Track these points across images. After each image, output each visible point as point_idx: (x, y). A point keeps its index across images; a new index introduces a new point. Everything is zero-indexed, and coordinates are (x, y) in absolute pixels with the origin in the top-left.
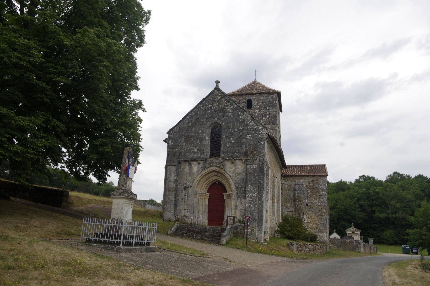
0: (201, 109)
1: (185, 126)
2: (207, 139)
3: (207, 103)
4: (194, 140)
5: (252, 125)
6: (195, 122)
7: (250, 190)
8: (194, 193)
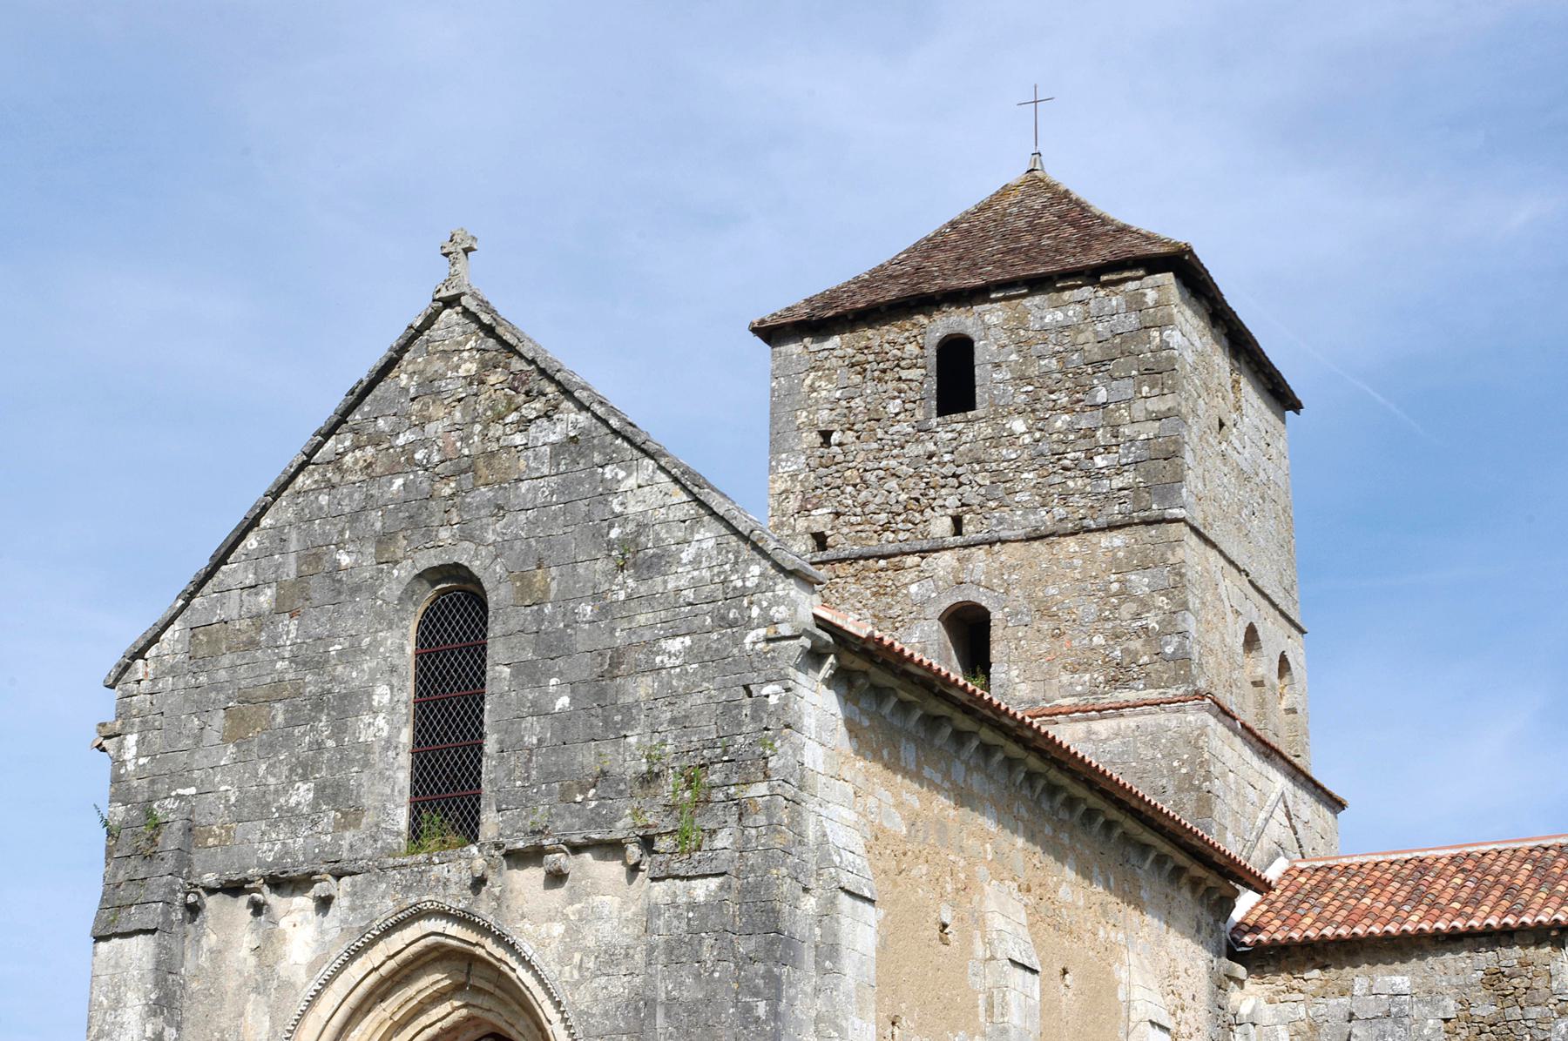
1: (235, 615)
2: (386, 699)
5: (696, 562)
6: (300, 576)
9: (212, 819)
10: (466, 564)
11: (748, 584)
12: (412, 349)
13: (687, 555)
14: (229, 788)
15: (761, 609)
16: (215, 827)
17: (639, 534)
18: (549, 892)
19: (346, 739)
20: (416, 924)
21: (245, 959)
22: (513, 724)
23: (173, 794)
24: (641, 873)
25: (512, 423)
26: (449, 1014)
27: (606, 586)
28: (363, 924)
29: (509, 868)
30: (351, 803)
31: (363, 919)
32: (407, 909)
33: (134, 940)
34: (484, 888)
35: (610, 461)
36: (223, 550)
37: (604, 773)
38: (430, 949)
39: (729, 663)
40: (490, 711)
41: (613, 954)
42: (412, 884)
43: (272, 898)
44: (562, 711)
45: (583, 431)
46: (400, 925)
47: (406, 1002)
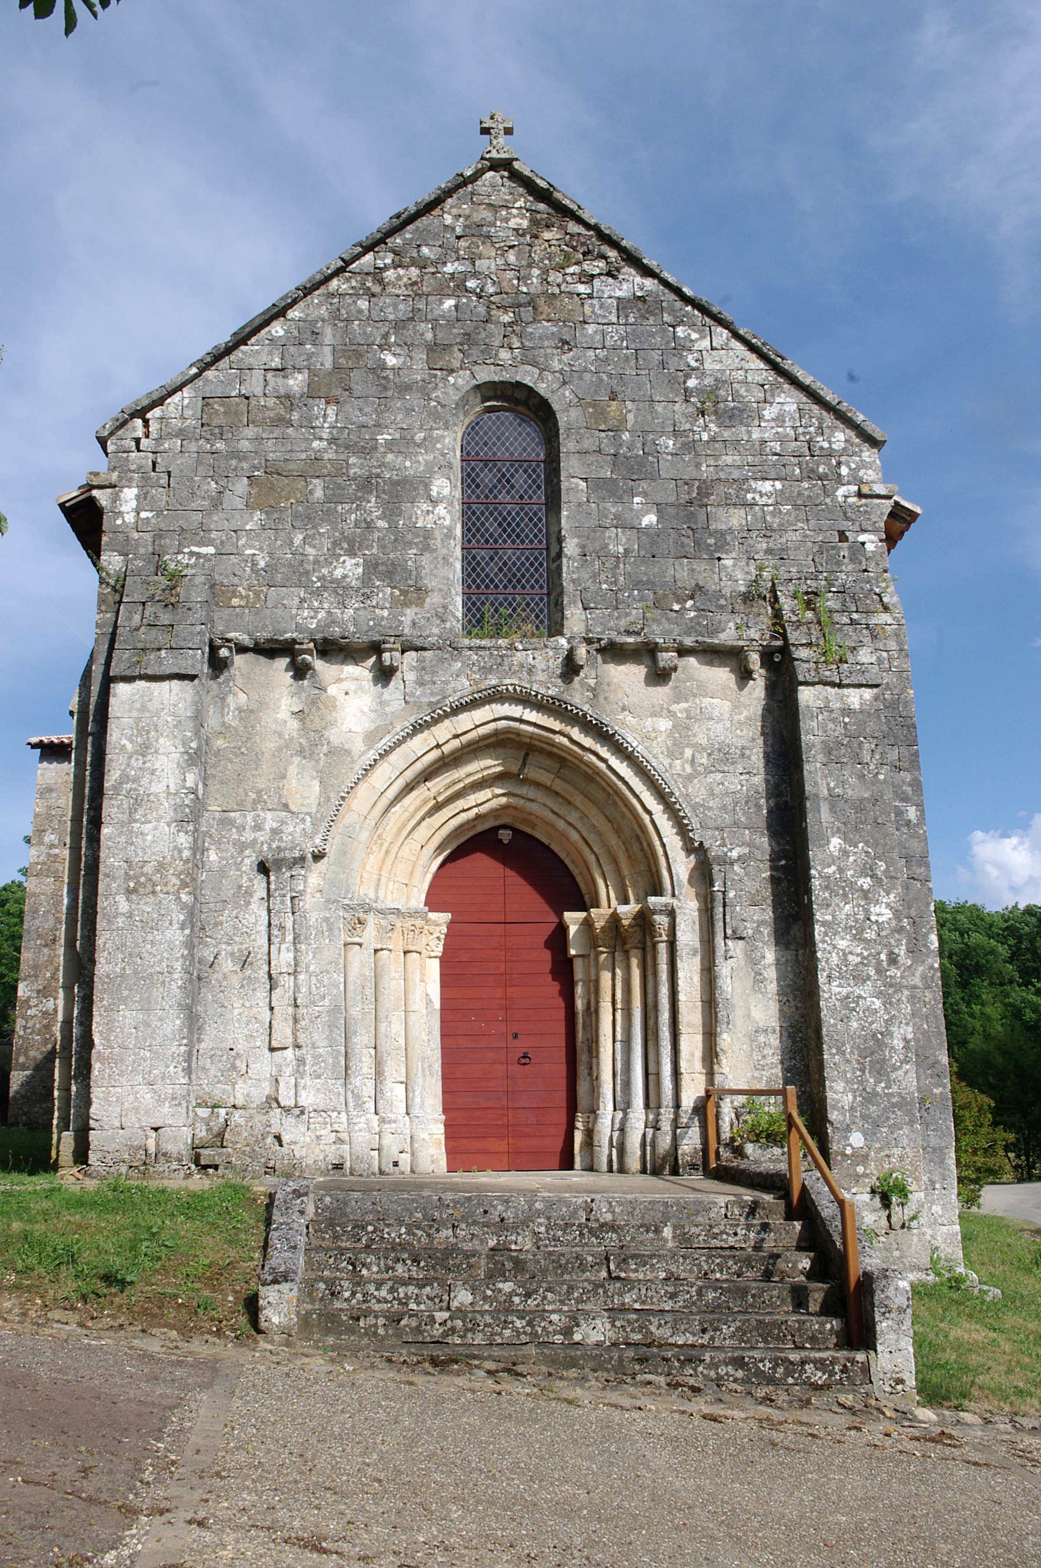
0: (381, 281)
1: (258, 391)
3: (425, 250)
4: (334, 497)
5: (779, 420)
6: (337, 368)
7: (841, 870)
8: (347, 908)
9: (236, 580)
10: (530, 384)
11: (834, 446)
12: (455, 196)
13: (769, 413)
14: (257, 552)
15: (850, 469)
16: (240, 588)
17: (718, 388)
19: (401, 522)
20: (487, 707)
21: (285, 722)
22: (595, 532)
23: (186, 550)
24: (751, 682)
25: (574, 274)
26: (488, 800)
27: (688, 426)
28: (433, 699)
29: (605, 662)
30: (411, 582)
31: (432, 694)
32: (486, 690)
33: (166, 685)
34: (577, 679)
35: (681, 323)
36: (248, 329)
37: (699, 588)
38: (496, 733)
39: (823, 510)
40: (568, 517)
41: (728, 753)
43: (319, 664)
44: (649, 527)
45: (650, 293)
46: (474, 704)
47: (454, 783)
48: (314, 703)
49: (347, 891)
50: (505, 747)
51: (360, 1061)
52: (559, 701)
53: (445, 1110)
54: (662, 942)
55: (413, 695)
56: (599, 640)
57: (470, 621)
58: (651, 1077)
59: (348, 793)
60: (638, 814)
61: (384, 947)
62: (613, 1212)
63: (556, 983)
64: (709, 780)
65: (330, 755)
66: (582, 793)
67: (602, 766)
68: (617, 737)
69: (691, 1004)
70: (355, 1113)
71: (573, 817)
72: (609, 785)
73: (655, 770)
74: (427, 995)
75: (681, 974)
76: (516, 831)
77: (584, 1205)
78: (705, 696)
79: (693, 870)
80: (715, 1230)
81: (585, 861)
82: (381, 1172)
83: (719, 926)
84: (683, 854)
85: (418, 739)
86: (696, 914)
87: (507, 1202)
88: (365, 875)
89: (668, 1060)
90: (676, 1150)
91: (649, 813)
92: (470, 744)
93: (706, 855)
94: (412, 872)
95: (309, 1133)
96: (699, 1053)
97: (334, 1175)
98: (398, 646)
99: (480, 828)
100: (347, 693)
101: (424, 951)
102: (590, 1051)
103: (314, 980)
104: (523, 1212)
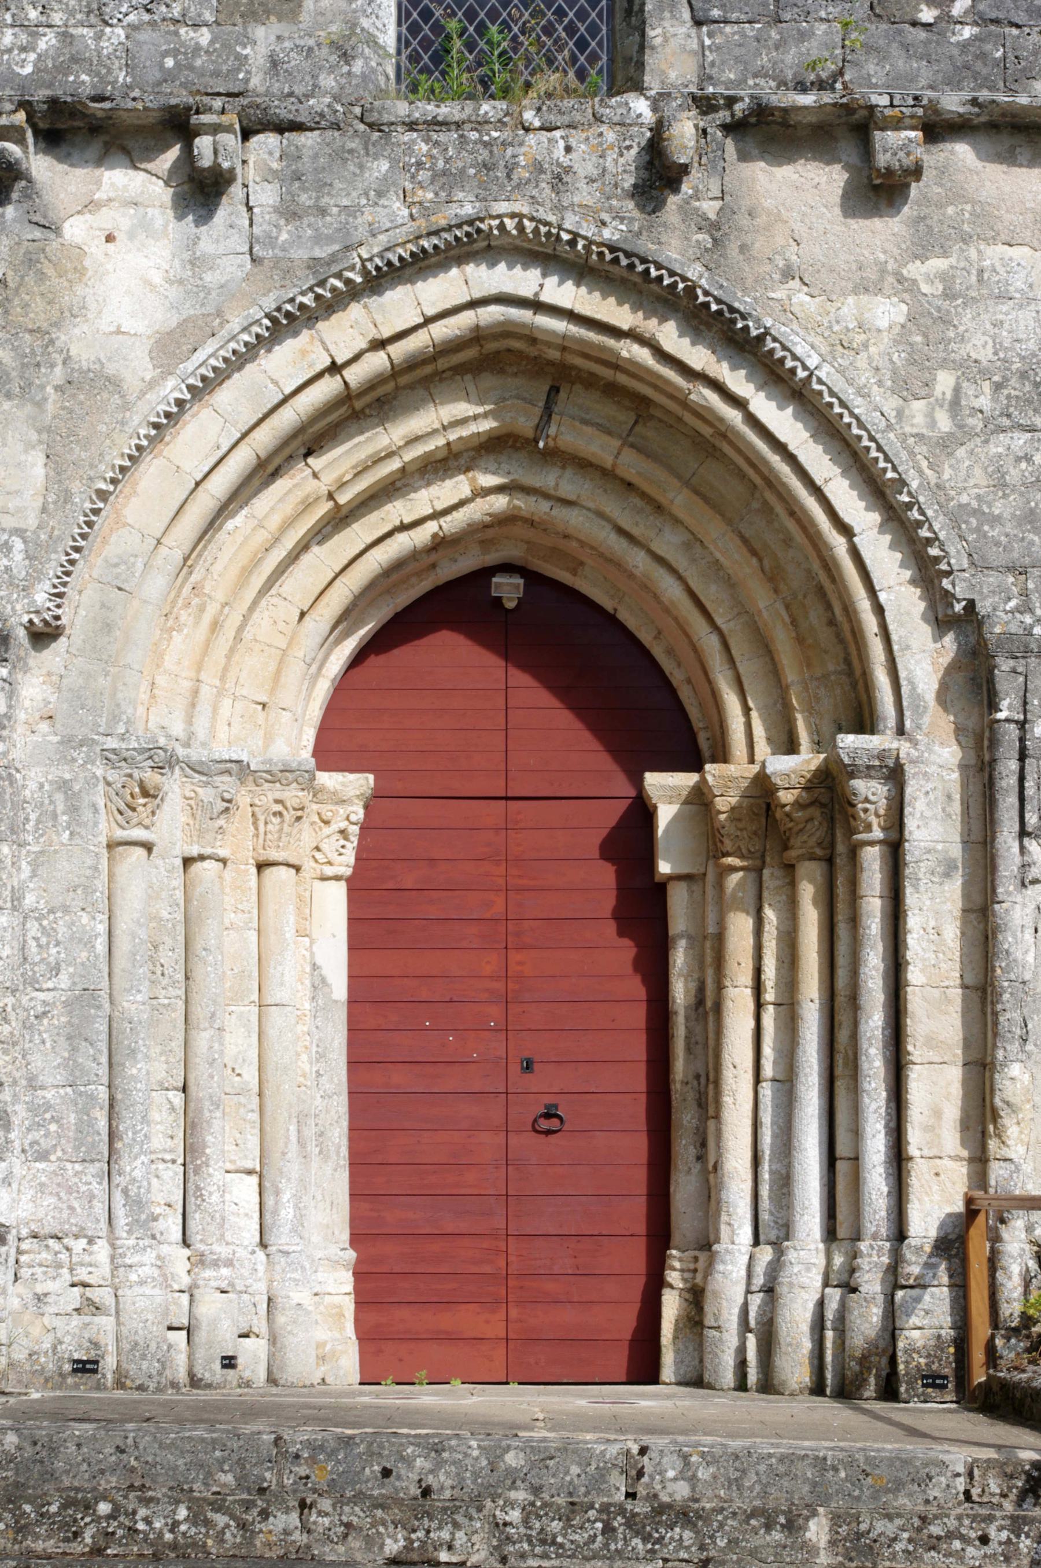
8: (113, 758)
18: (857, 225)
20: (454, 271)
26: (462, 503)
28: (319, 253)
29: (744, 157)
31: (318, 239)
32: (449, 228)
34: (673, 201)
38: (477, 336)
42: (462, 171)
47: (378, 460)
48: (30, 261)
49: (115, 719)
50: (502, 371)
51: (145, 1120)
52: (628, 255)
53: (356, 1239)
54: (871, 843)
55: (270, 241)
56: (731, 101)
57: (414, 58)
58: (841, 1166)
59: (114, 481)
60: (819, 534)
61: (207, 851)
62: (693, 1480)
63: (627, 942)
64: (994, 449)
65: (70, 390)
66: (687, 484)
67: (733, 416)
68: (770, 344)
69: (936, 993)
70: (132, 1242)
71: (668, 543)
72: (753, 465)
73: (861, 425)
74: (315, 967)
75: (914, 922)
76: (533, 578)
77: (621, 1461)
78: (993, 240)
79: (951, 669)
80: (936, 1530)
81: (695, 649)
82: (194, 1381)
83: (1008, 803)
84: (926, 630)
85: (287, 350)
86: (956, 775)
87: (438, 1449)
88: (161, 680)
89: (880, 1126)
90: (894, 1339)
91: (846, 530)
92: (413, 363)
93: (980, 634)
94: (278, 672)
95: (20, 1288)
96: (952, 1111)
97: (76, 1386)
98: (231, 119)
99: (450, 570)
100: (110, 238)
101: (308, 865)
102: (702, 1104)
103: (33, 928)
104: (476, 1475)
